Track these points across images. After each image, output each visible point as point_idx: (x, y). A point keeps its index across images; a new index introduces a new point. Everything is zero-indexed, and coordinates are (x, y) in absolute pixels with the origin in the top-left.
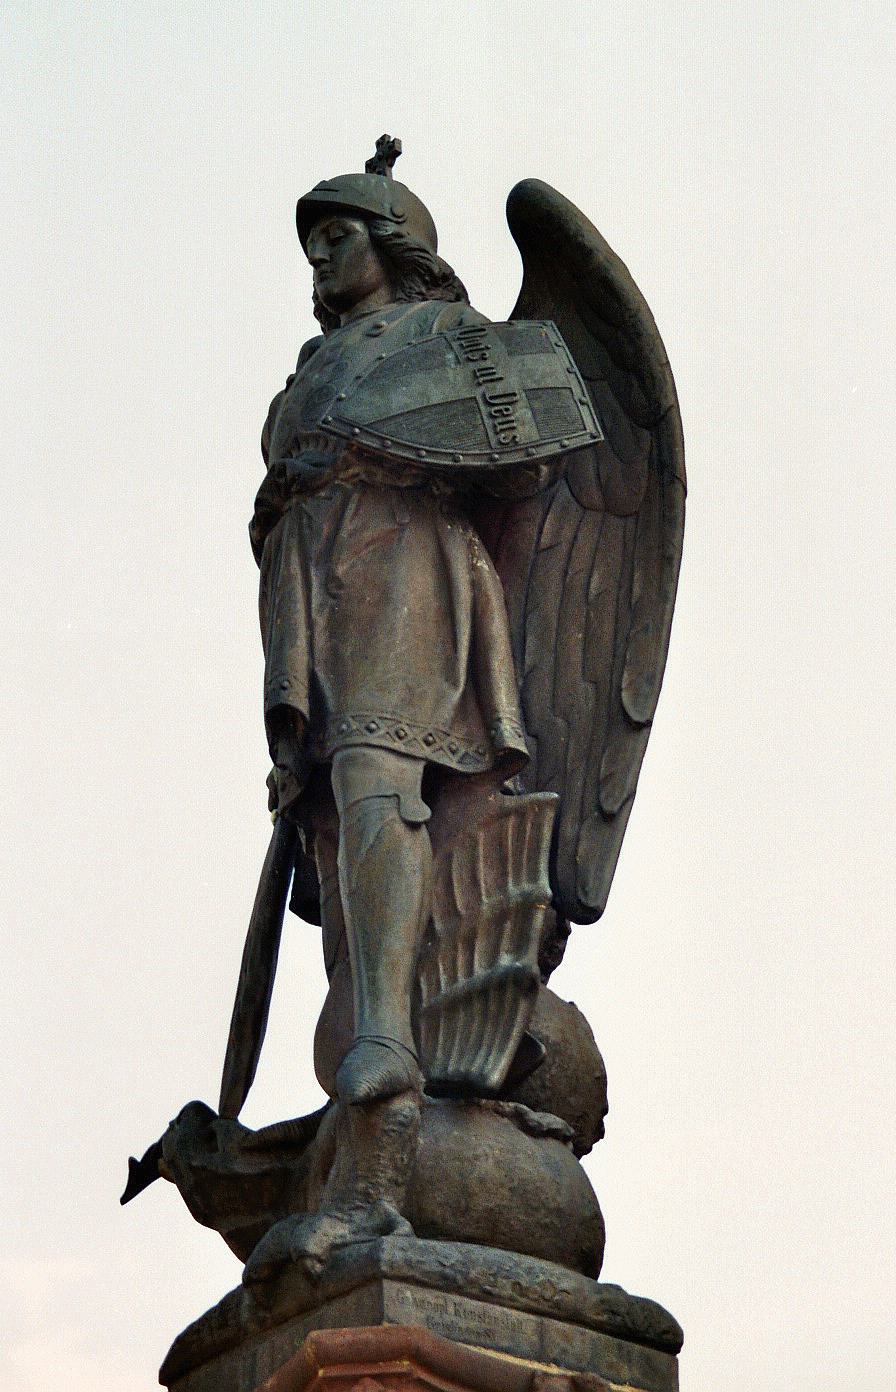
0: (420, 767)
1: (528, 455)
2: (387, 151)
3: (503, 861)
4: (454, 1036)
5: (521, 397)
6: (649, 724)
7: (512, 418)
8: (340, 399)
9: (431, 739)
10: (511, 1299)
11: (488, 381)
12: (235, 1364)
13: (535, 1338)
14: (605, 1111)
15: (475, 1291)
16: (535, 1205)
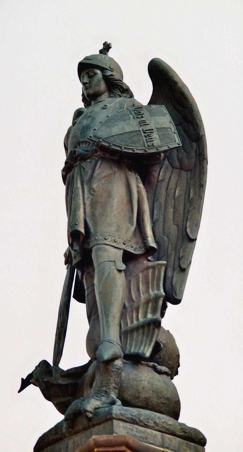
0: (122, 252)
1: (157, 150)
2: (107, 47)
3: (148, 283)
4: (133, 340)
5: (155, 130)
6: (196, 239)
7: (152, 137)
8: (95, 129)
9: (125, 243)
10: (153, 427)
11: (144, 125)
12: (61, 446)
13: (161, 440)
14: (179, 366)
15: (142, 424)
16: (161, 396)
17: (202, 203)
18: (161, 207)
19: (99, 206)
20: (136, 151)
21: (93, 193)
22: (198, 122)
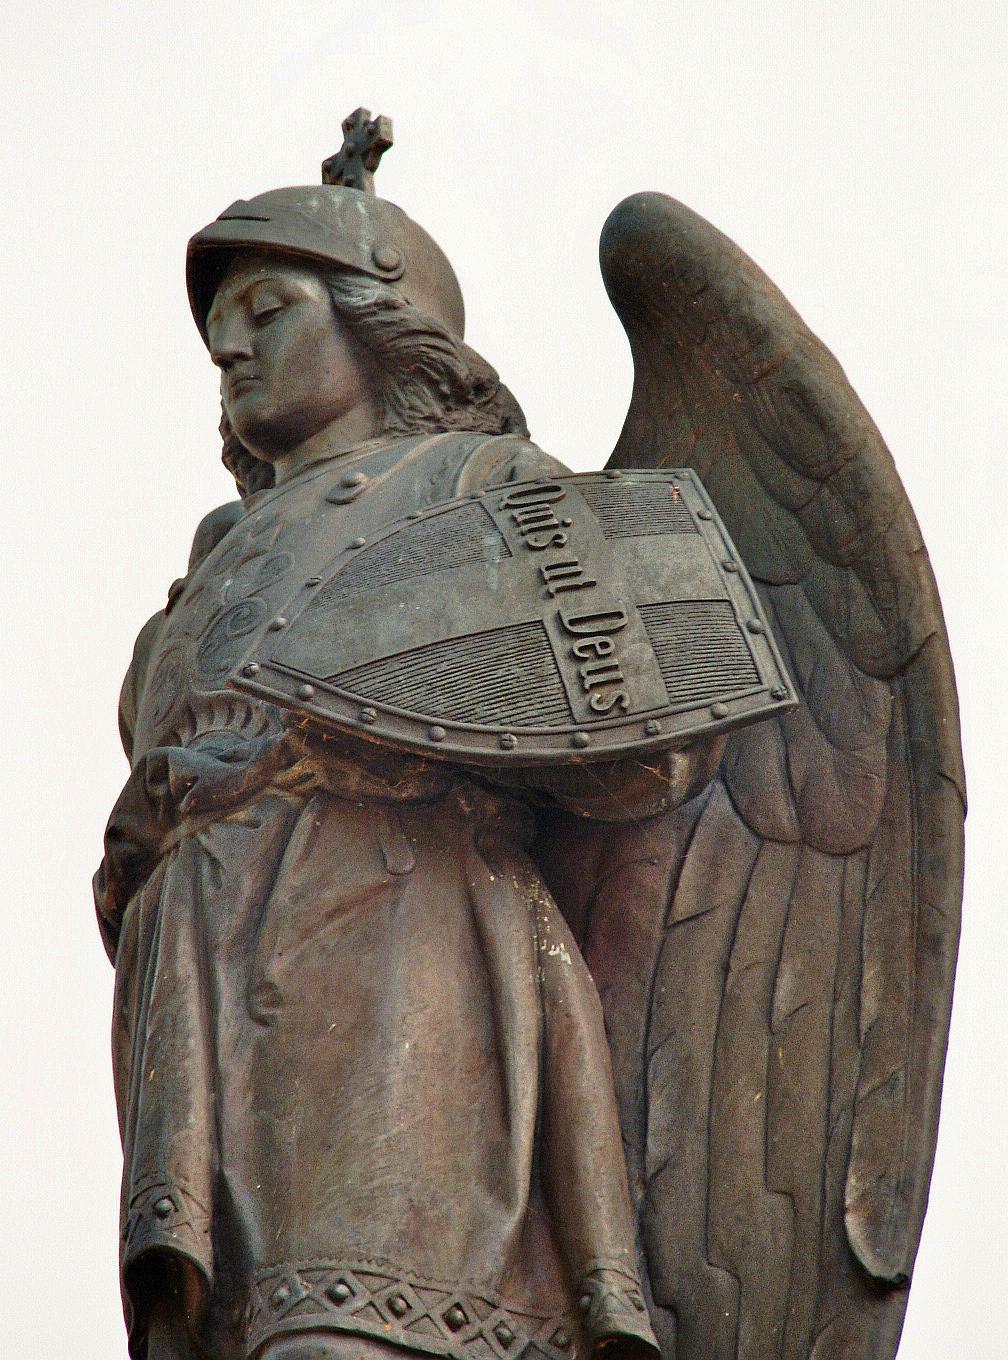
1: (649, 734)
6: (903, 1283)
7: (615, 661)
8: (276, 628)
17: (934, 1051)
18: (686, 1084)
19: (300, 1088)
20: (521, 748)
21: (264, 1011)
22: (902, 560)
